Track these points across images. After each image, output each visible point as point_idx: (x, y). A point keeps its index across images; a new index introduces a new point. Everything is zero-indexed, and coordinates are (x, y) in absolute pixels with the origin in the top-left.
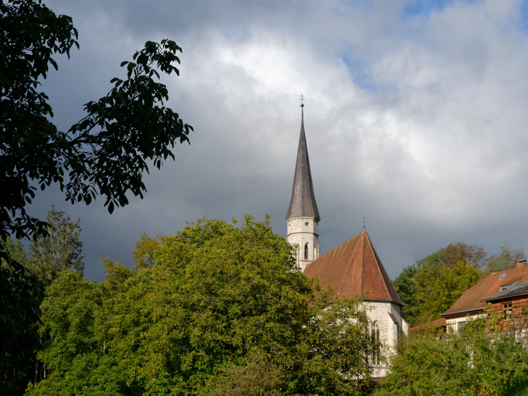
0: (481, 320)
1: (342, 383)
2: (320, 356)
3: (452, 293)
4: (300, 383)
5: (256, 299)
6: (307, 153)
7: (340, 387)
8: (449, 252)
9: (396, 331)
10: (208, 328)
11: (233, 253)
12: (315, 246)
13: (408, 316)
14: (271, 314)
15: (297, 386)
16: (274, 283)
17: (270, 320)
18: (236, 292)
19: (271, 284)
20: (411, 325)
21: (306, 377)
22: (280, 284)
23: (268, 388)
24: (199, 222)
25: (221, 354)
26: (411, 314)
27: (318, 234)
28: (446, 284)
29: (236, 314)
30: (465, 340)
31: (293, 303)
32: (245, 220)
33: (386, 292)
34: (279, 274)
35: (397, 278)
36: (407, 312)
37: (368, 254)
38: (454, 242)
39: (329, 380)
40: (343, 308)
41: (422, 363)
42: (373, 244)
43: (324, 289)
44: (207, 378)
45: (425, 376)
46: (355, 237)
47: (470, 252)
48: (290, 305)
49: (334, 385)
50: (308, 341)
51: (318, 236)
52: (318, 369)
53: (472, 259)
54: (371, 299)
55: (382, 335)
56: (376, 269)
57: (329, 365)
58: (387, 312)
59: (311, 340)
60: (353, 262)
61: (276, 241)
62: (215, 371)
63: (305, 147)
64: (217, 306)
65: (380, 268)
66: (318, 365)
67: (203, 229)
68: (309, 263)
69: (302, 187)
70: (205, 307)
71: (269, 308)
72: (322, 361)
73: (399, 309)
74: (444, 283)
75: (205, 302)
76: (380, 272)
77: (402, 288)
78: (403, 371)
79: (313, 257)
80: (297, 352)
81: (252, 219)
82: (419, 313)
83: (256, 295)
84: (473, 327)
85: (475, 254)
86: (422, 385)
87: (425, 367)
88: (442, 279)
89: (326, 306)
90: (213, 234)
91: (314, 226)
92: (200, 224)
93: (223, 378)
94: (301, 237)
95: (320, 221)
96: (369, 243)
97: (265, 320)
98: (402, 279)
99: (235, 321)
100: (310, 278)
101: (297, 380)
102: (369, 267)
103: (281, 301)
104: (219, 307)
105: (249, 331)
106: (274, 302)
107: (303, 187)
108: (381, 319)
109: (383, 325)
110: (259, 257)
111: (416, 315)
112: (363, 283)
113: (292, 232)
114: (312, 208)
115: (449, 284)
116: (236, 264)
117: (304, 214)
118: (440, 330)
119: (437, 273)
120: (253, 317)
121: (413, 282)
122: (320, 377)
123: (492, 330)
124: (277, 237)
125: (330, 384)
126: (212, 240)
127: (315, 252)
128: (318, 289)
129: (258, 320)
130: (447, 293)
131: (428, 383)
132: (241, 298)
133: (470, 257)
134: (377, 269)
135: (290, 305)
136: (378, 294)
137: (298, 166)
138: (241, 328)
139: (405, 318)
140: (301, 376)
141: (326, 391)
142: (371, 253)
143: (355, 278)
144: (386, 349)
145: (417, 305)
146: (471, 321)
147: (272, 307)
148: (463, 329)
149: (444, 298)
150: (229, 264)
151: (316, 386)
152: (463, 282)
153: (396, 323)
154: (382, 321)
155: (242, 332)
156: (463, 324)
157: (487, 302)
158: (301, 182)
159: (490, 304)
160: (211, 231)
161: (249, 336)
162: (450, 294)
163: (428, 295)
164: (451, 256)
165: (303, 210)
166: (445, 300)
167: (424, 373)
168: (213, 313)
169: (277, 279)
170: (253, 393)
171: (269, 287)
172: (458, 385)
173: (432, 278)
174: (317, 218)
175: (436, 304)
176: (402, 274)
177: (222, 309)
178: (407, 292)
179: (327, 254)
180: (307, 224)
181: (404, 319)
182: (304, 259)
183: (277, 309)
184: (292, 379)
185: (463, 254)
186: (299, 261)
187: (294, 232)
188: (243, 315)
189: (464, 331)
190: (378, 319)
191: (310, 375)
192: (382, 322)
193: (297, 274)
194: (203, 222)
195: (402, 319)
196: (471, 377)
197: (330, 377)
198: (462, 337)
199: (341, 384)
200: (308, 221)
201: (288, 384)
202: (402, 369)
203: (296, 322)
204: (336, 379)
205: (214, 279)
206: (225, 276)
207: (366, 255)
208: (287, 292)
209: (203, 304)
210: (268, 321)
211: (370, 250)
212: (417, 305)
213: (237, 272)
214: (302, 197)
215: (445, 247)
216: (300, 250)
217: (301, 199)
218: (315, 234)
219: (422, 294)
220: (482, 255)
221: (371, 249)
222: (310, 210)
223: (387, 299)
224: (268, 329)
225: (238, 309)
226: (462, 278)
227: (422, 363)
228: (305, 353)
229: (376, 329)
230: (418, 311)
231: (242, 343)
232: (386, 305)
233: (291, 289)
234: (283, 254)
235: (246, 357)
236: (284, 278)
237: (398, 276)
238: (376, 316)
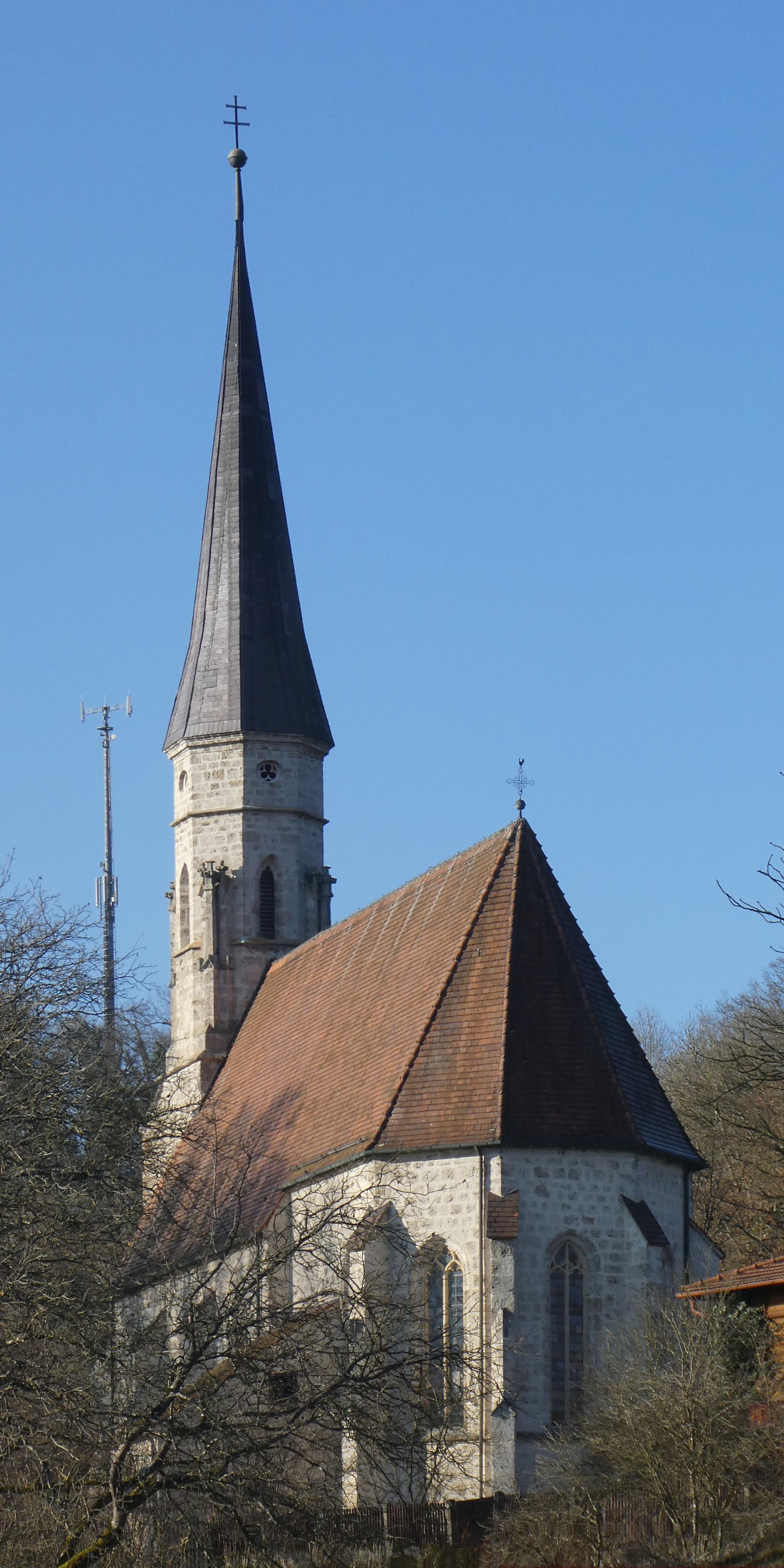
51: (327, 822)
58: (617, 1197)
73: (680, 1181)
108: (589, 1227)
238: (567, 1213)
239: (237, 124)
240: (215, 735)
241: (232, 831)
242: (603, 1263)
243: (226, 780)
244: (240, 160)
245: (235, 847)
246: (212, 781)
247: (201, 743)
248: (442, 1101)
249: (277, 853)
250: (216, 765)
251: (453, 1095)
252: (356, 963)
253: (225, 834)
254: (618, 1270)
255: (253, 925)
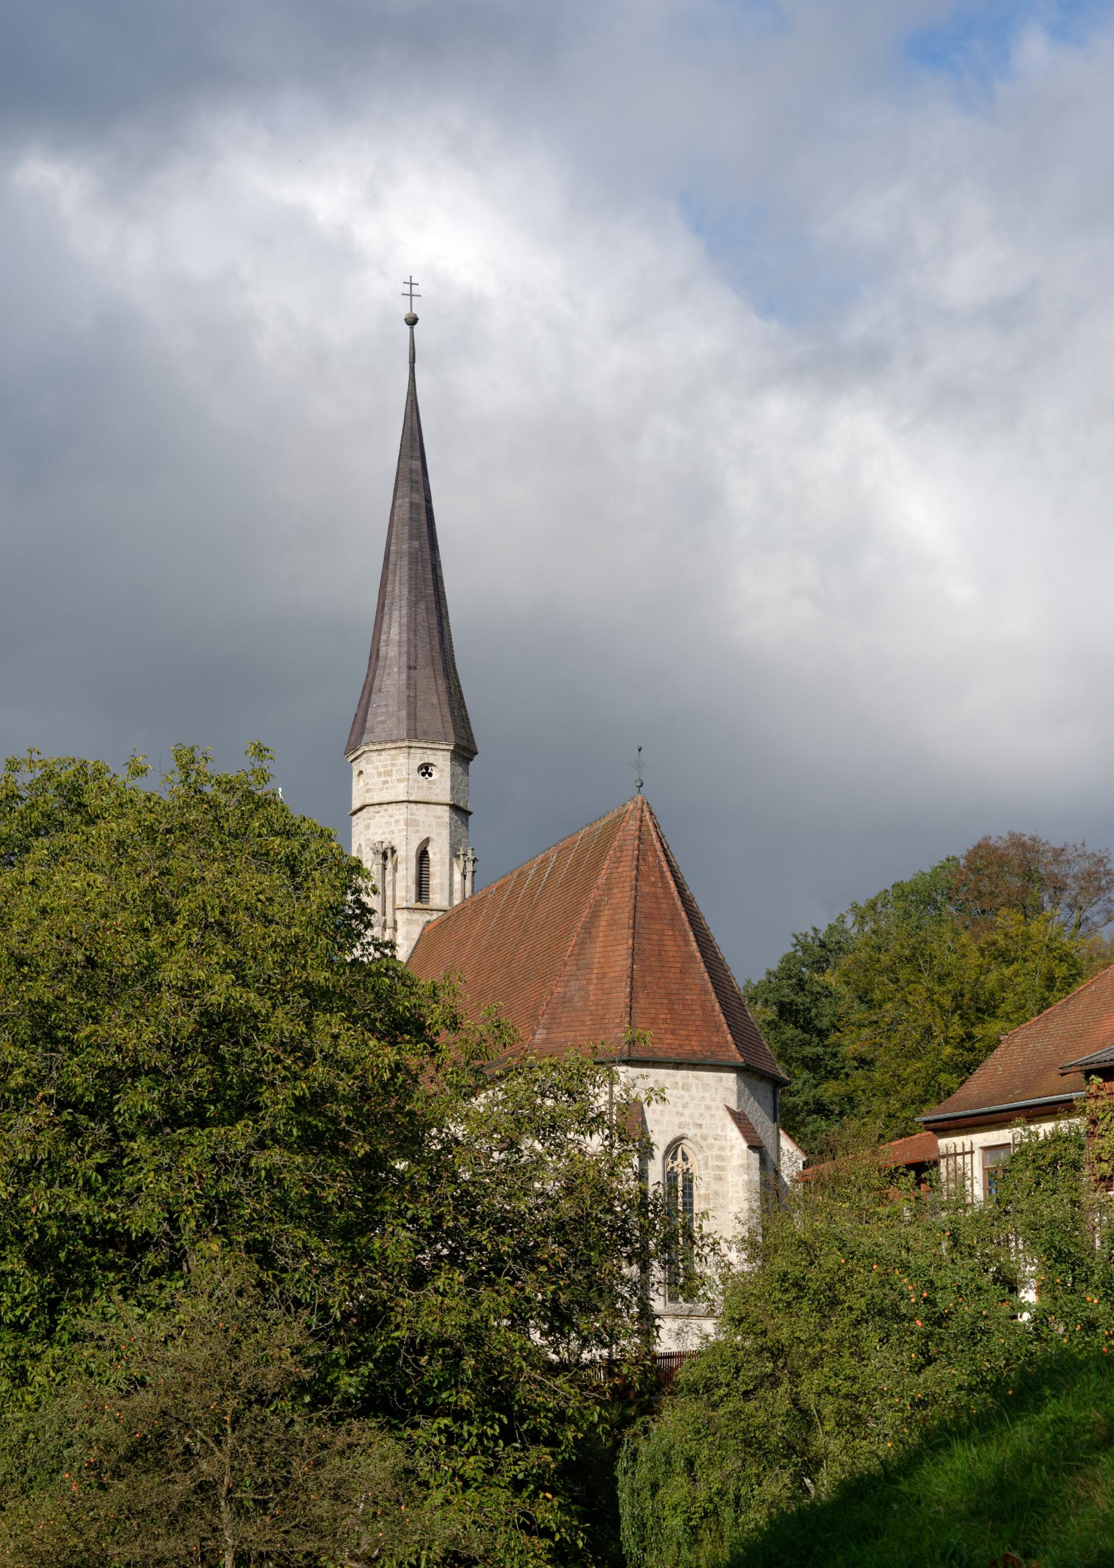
0: (1067, 1139)
1: (539, 1378)
2: (459, 1277)
3: (977, 1031)
4: (383, 1375)
5: (218, 1060)
6: (428, 500)
7: (530, 1391)
8: (977, 871)
9: (756, 1176)
10: (38, 1170)
11: (133, 890)
12: (454, 855)
13: (810, 1119)
14: (275, 1117)
15: (370, 1386)
16: (286, 1002)
17: (269, 1142)
18: (145, 1037)
19: (274, 1006)
20: (815, 1152)
21: (402, 1351)
22: (310, 1005)
23: (253, 1398)
24: (13, 766)
25: (89, 1266)
26: (821, 1109)
27: (469, 809)
28: (954, 998)
29: (143, 1117)
30: (1007, 1213)
31: (355, 1078)
32: (174, 765)
33: (718, 1028)
34: (304, 967)
35: (769, 973)
36: (806, 1103)
37: (653, 884)
38: (998, 833)
39: (490, 1366)
40: (544, 1095)
41: (834, 1302)
42: (673, 850)
43: (475, 1025)
44: (36, 1357)
45: (846, 1353)
46: (607, 819)
47: (1055, 868)
48: (345, 1085)
49: (513, 1385)
50: (414, 1219)
51: (470, 813)
52: (452, 1326)
53: (1066, 898)
54: (661, 1055)
55: (702, 1191)
56: (681, 943)
57: (489, 1310)
58: (722, 1106)
59: (426, 1214)
60: (595, 915)
61: (296, 845)
62: (63, 1329)
63: (420, 477)
64: (72, 1089)
65: (697, 941)
66: (450, 1309)
67: (24, 795)
68: (435, 916)
69: (409, 630)
70: (28, 1091)
71: (266, 1096)
72: (464, 1293)
73: (770, 1095)
74: (948, 992)
75: (26, 1075)
76: (698, 954)
77: (790, 1012)
78: (764, 1333)
79: (447, 895)
80: (373, 1259)
81: (203, 763)
82: (853, 1108)
83: (217, 1047)
84: (1039, 1168)
85: (1075, 877)
86: (833, 1384)
87: (846, 1320)
88: (941, 980)
89: (484, 1088)
90: (63, 816)
91: (453, 775)
92: (16, 776)
93: (93, 1356)
94: (402, 818)
95: (476, 758)
96: (658, 845)
97: (251, 1140)
98: (790, 977)
99: (139, 1146)
100: (426, 982)
101: (371, 1365)
102: (655, 937)
103: (310, 1070)
104: (80, 1091)
105: (191, 1180)
106: (284, 1073)
107: (413, 628)
108: (699, 1132)
109: (708, 1153)
110: (231, 905)
111: (841, 1114)
112: (632, 996)
113: (368, 802)
114: (446, 710)
115: (968, 996)
116: (146, 932)
117: (415, 733)
118: (903, 1179)
119: (923, 955)
120: (207, 1130)
121: (831, 988)
122: (459, 1355)
123: (1103, 1179)
124: (305, 826)
125: (494, 1381)
126: (59, 840)
127: (457, 877)
128: (454, 1024)
129: (227, 1142)
130: (957, 1029)
131: (854, 1379)
132: (159, 1058)
133: (1060, 889)
134: (686, 942)
135: (345, 1085)
136: (688, 1038)
137: (393, 548)
138: (158, 1170)
139: (793, 1132)
140: (383, 1351)
141: (478, 1405)
142: (665, 884)
143: (604, 975)
144: (707, 1250)
145: (847, 1075)
146: (1029, 1145)
147: (276, 1093)
148: (1000, 1175)
149: (948, 1050)
150: (117, 932)
151: (442, 1387)
152: (1019, 989)
153: (755, 1146)
154: (704, 1138)
155: (163, 1186)
156: (1003, 1155)
157: (1088, 1074)
158: (404, 611)
159: (1097, 1080)
160: (58, 802)
161: (190, 1202)
162: (970, 1036)
163: (888, 1038)
164: (986, 886)
165: (412, 716)
166: (951, 1057)
167: (841, 1341)
168: (57, 1113)
169: (296, 987)
170: (199, 1413)
171: (267, 1019)
172: (960, 1388)
173: (904, 974)
174: (464, 749)
175: (918, 1071)
176: (788, 959)
177: (90, 1098)
178: (808, 1027)
179: (498, 883)
180: (425, 770)
181: (787, 1133)
182: (412, 903)
183: (298, 1100)
184: (352, 1362)
185: (1029, 875)
186: (395, 910)
187: (376, 801)
188: (174, 1120)
189: (1003, 1180)
190: (690, 1132)
191: (417, 1347)
192: (703, 1144)
193: (373, 968)
194: (25, 768)
195: (781, 1132)
196: (1007, 1360)
197: (495, 1353)
198: (998, 1202)
199: (535, 1381)
200: (429, 757)
201: (337, 1379)
202: (759, 1327)
203: (368, 1148)
204: (517, 1361)
205: (62, 988)
206: (102, 974)
207: (646, 889)
208: (335, 1037)
209: (20, 1080)
210: (261, 1145)
211: (662, 872)
212: (847, 1075)
213: (146, 963)
214: (409, 668)
215: (960, 849)
216: (401, 867)
217: (404, 676)
218: (455, 808)
219: (866, 1032)
220: (1103, 882)
221: (666, 868)
222: (437, 716)
223: (723, 1057)
224: (263, 1173)
225: (152, 1101)
226: (1016, 974)
227: (834, 1302)
228: (401, 1266)
229: (679, 1165)
230: (851, 1100)
231: (166, 1226)
232: (721, 1079)
233: (347, 1025)
234: (320, 895)
235: (182, 1277)
236: (322, 982)
237: (775, 967)
238: (682, 1120)
239: (411, 295)
240: (386, 742)
241: (398, 817)
242: (710, 1163)
243: (394, 778)
244: (412, 321)
245: (400, 831)
246: (383, 779)
247: (375, 748)
248: (577, 1024)
249: (432, 836)
250: (386, 766)
251: (588, 1018)
252: (500, 918)
253: (392, 820)
254: (722, 1168)
255: (413, 893)
